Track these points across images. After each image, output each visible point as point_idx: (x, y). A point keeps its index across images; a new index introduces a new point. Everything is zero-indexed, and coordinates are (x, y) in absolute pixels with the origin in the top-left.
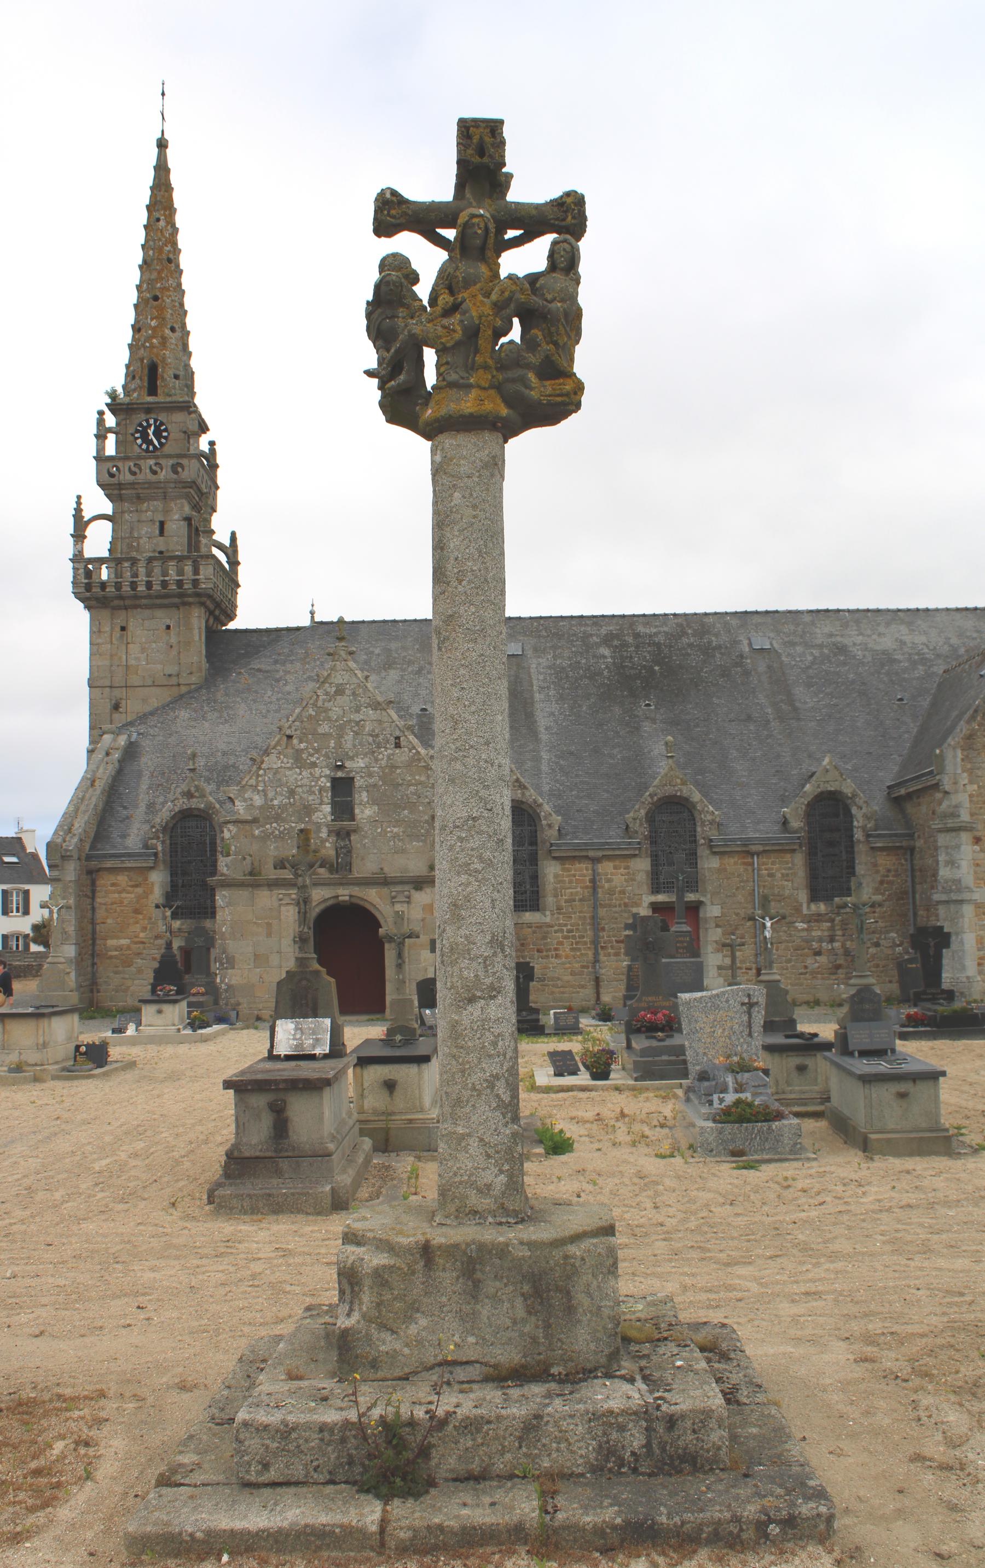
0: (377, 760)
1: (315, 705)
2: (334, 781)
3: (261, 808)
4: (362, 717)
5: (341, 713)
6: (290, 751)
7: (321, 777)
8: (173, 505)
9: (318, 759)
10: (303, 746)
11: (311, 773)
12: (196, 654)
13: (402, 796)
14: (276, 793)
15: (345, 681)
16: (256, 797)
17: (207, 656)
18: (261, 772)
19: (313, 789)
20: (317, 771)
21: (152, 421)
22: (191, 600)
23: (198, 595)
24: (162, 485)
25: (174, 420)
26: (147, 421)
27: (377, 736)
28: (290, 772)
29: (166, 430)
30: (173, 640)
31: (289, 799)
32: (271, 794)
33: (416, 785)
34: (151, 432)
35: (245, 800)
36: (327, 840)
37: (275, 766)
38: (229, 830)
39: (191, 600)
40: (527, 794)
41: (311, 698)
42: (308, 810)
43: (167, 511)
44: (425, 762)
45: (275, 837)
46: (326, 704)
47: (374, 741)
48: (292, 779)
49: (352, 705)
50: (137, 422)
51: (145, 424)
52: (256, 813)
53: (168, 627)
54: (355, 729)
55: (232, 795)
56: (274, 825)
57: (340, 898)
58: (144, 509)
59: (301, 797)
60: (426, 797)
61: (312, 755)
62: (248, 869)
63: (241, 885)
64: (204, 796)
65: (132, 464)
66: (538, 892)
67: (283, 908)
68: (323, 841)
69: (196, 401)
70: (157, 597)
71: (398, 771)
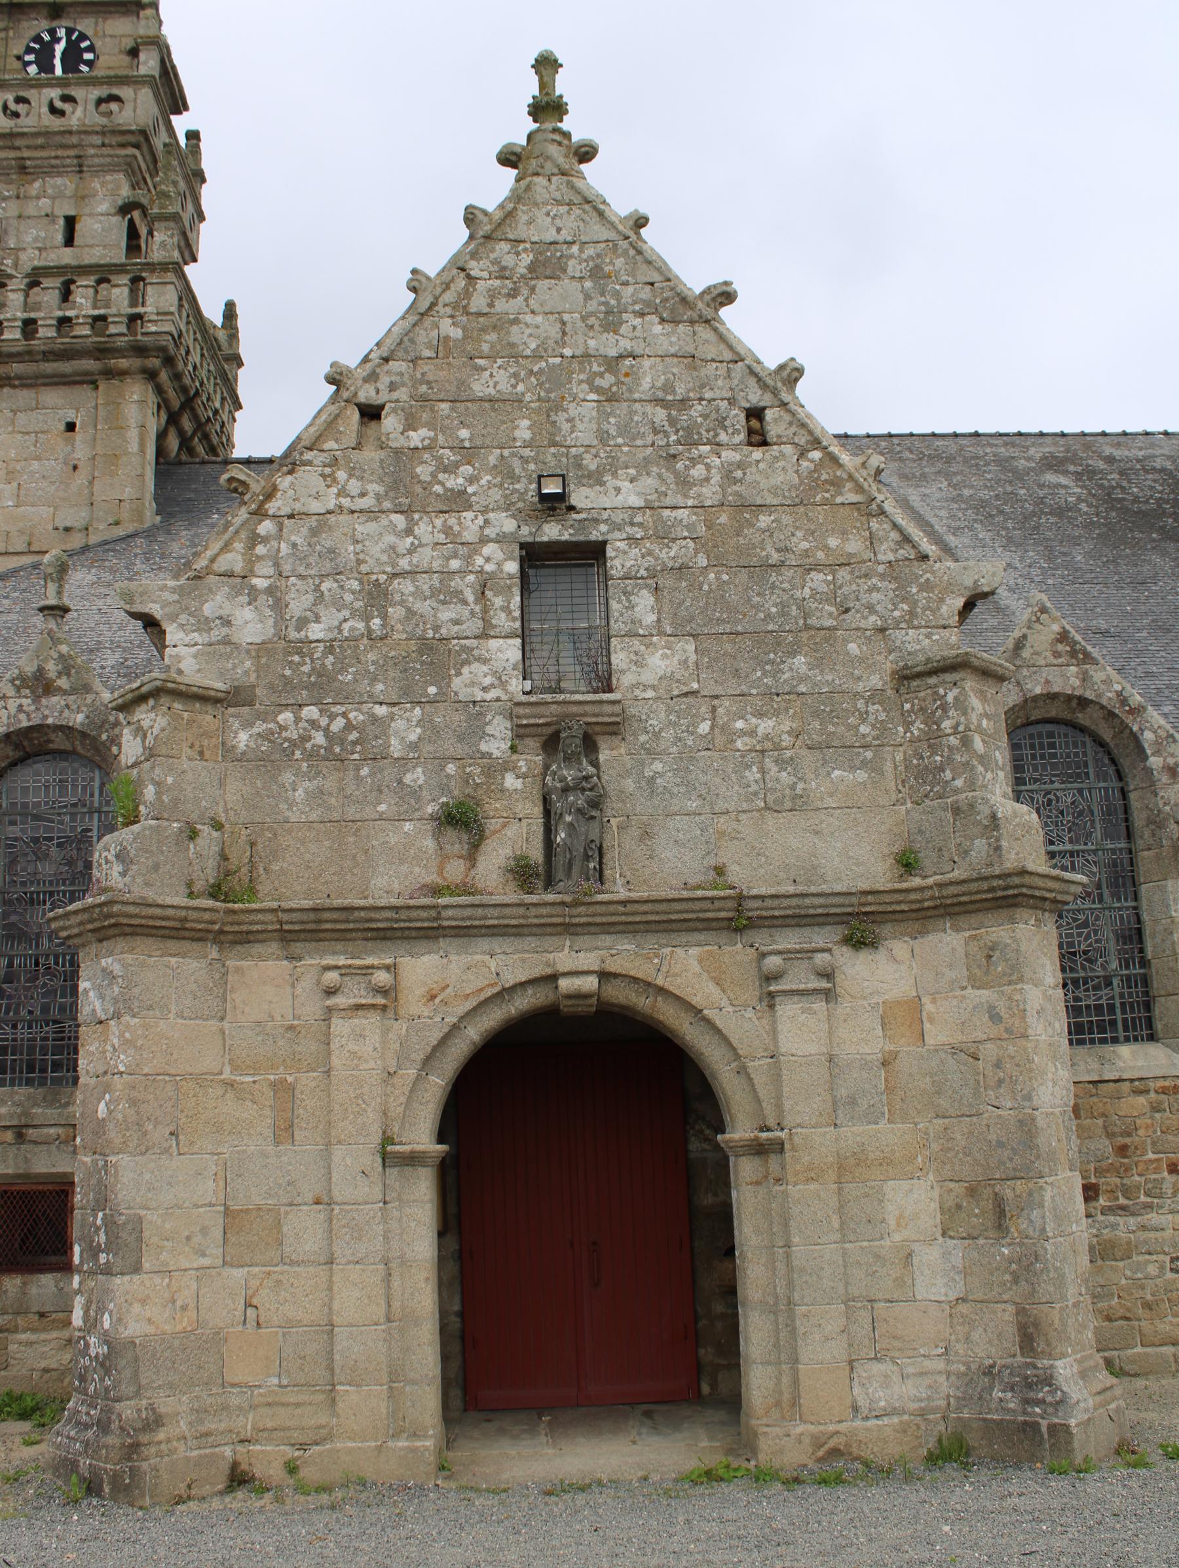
0: (684, 483)
1: (461, 307)
2: (535, 557)
3: (261, 650)
4: (626, 344)
5: (554, 331)
6: (370, 455)
7: (484, 540)
8: (96, 184)
9: (472, 480)
10: (416, 438)
11: (447, 530)
12: (132, 480)
13: (783, 605)
14: (320, 597)
15: (565, 235)
16: (248, 613)
17: (156, 497)
18: (266, 527)
19: (456, 583)
20: (470, 524)
21: (61, 33)
22: (123, 363)
23: (140, 350)
24: (74, 140)
25: (109, 31)
26: (53, 32)
27: (684, 403)
28: (371, 527)
29: (91, 49)
30: (81, 453)
31: (367, 619)
32: (298, 604)
33: (833, 567)
34: (59, 48)
35: (203, 625)
36: (508, 767)
37: (316, 507)
38: (140, 732)
39: (123, 363)
40: (1098, 676)
41: (447, 287)
42: (436, 656)
43: (83, 198)
44: (859, 489)
45: (310, 756)
46: (501, 305)
47: (672, 421)
48: (376, 551)
49: (592, 306)
50: (33, 33)
51: (46, 37)
52: (244, 670)
53: (71, 427)
54: (607, 381)
55: (155, 610)
56: (310, 712)
57: (564, 984)
58: (34, 193)
59: (411, 613)
60: (871, 608)
61: (451, 469)
62: (207, 873)
63: (172, 930)
64: (87, 688)
65: (10, 97)
66: (1145, 981)
67: (339, 1026)
68: (494, 769)
69: (165, 30)
70: (51, 355)
71: (764, 520)
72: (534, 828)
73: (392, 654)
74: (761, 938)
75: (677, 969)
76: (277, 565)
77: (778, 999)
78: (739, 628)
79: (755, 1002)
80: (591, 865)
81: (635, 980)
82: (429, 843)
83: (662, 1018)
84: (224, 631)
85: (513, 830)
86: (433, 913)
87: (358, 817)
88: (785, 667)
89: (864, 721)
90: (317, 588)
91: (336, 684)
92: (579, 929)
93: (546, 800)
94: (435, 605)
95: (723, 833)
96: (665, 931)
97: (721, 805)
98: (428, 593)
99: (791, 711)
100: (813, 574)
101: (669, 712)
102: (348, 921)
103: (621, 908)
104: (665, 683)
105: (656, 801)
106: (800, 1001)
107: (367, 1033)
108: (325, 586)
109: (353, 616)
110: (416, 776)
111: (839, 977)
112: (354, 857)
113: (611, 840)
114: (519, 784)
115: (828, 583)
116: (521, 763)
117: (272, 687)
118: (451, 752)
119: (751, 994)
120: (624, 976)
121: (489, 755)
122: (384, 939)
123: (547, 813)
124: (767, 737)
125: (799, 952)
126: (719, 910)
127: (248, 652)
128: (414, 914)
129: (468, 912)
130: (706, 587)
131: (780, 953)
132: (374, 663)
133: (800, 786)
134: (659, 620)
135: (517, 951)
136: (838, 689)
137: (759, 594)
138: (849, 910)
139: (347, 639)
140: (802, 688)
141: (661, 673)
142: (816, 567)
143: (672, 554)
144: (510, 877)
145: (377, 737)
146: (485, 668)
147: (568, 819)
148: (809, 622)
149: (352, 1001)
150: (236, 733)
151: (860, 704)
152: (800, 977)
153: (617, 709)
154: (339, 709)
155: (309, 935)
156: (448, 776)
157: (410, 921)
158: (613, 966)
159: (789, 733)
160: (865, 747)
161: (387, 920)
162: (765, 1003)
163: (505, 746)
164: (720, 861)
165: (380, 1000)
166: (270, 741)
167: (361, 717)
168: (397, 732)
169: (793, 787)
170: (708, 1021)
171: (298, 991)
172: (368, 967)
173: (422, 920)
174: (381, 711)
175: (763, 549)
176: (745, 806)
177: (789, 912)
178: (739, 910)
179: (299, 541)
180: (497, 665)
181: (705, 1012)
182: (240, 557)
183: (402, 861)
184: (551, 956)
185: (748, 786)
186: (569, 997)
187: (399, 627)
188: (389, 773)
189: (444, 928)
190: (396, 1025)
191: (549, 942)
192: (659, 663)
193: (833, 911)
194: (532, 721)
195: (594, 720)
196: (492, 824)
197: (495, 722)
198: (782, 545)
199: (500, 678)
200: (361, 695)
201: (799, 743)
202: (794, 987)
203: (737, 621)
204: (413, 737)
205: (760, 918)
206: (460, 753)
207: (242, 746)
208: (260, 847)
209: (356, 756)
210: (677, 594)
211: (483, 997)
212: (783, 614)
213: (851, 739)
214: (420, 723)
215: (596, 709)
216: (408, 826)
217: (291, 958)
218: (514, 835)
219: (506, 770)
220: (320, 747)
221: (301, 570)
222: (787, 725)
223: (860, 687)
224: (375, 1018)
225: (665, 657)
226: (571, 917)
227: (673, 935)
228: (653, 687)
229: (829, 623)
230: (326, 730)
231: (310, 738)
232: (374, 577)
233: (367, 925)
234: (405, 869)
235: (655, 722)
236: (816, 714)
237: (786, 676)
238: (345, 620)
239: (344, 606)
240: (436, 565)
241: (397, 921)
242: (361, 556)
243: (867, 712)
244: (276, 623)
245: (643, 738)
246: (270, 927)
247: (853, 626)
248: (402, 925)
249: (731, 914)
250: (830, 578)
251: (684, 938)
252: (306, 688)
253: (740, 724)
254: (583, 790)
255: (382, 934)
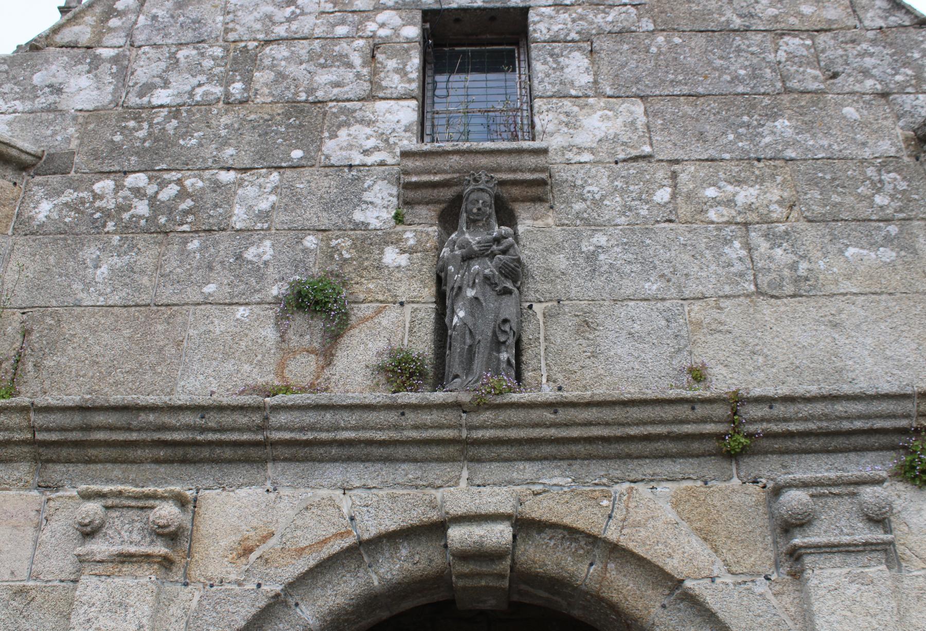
16: (85, 81)
31: (226, 82)
36: (387, 239)
42: (307, 117)
52: (64, 137)
56: (139, 180)
59: (281, 76)
60: (866, 73)
67: (92, 589)
68: (369, 242)
72: (421, 315)
73: (252, 117)
74: (771, 470)
75: (638, 515)
76: (130, 35)
77: (808, 560)
78: (701, 90)
79: (767, 568)
80: (504, 356)
81: (572, 532)
82: (269, 333)
83: (615, 597)
84: (52, 99)
85: (390, 317)
86: (257, 419)
87: (175, 299)
88: (765, 130)
89: (879, 191)
90: (173, 56)
91: (176, 149)
92: (483, 451)
93: (440, 281)
94: (312, 68)
95: (699, 324)
96: (618, 457)
97: (692, 289)
98: (305, 57)
99: (779, 179)
100: (786, 39)
101: (613, 177)
102: (129, 429)
103: (548, 416)
104: (606, 146)
105: (599, 282)
106: (844, 564)
107: (131, 600)
108: (181, 55)
109: (209, 81)
110: (262, 250)
111: (899, 530)
112: (161, 350)
113: (535, 330)
114: (403, 260)
115: (808, 48)
116: (408, 235)
117: (95, 155)
118: (314, 222)
119: (761, 554)
120: (554, 526)
121: (365, 226)
122: (184, 461)
123: (441, 297)
124: (750, 207)
125: (835, 484)
126: (704, 420)
127: (75, 118)
128: (227, 419)
129: (310, 418)
130: (654, 49)
131: (805, 485)
132: (227, 126)
133: (803, 266)
134: (595, 82)
135: (385, 485)
136: (837, 155)
137: (721, 58)
138: (904, 423)
139: (197, 104)
140: (790, 153)
141: (600, 134)
142: (792, 32)
143: (610, 18)
144: (382, 378)
145: (216, 206)
146: (368, 131)
147: (470, 293)
148: (789, 84)
149: (115, 549)
150: (38, 202)
151: (871, 172)
152: (837, 524)
153: (540, 161)
154: (175, 175)
155: (73, 452)
156: (306, 251)
157: (221, 430)
158: (537, 510)
159: (780, 203)
160: (888, 220)
161: (189, 428)
162: (785, 569)
163: (388, 215)
164: (698, 360)
165: (160, 549)
166: (78, 211)
167: (200, 184)
168: (243, 199)
169: (794, 267)
170: (693, 602)
171: (45, 536)
172: (147, 497)
173: (240, 430)
174: (226, 177)
175: (721, 15)
176: (727, 289)
177: (812, 426)
178: (734, 419)
179: (160, 13)
180: (385, 127)
181: (688, 584)
182: (89, 29)
183: (227, 356)
184: (438, 494)
185: (730, 265)
186: (464, 556)
187: (266, 91)
188: (225, 245)
189: (275, 444)
190: (184, 593)
191: (435, 472)
192: (598, 124)
193: (879, 424)
194: (425, 178)
195: (510, 176)
196: (361, 311)
197: (376, 187)
198: (745, 11)
199: (387, 141)
200: (205, 160)
201: (794, 214)
202: (833, 539)
203: (697, 83)
204: (264, 205)
205: (769, 435)
206: (325, 223)
207: (41, 217)
208: (34, 337)
209: (186, 227)
210: (618, 56)
211: (327, 552)
212: (754, 76)
213: (863, 210)
214: (275, 190)
215: (514, 161)
216: (241, 312)
217: (44, 487)
218: (393, 321)
219: (387, 243)
220: (141, 217)
221: (158, 40)
222: (775, 194)
223: (867, 153)
224: (147, 576)
225: (604, 118)
226: (471, 428)
227: (632, 464)
228: (591, 150)
229: (814, 86)
230: (153, 200)
231: (130, 207)
232: (243, 44)
233: (157, 436)
234: (229, 366)
235: (595, 189)
236: (814, 182)
237: (768, 139)
238: (200, 85)
239: (202, 72)
240: (318, 32)
241: (203, 430)
242: (231, 25)
243: (881, 181)
244: (115, 90)
245: (578, 206)
246: (17, 436)
247: (846, 89)
248: (211, 436)
249: (721, 428)
250: (809, 42)
251: (648, 468)
252: (137, 154)
253: (711, 192)
254: (492, 256)
255: (180, 452)
